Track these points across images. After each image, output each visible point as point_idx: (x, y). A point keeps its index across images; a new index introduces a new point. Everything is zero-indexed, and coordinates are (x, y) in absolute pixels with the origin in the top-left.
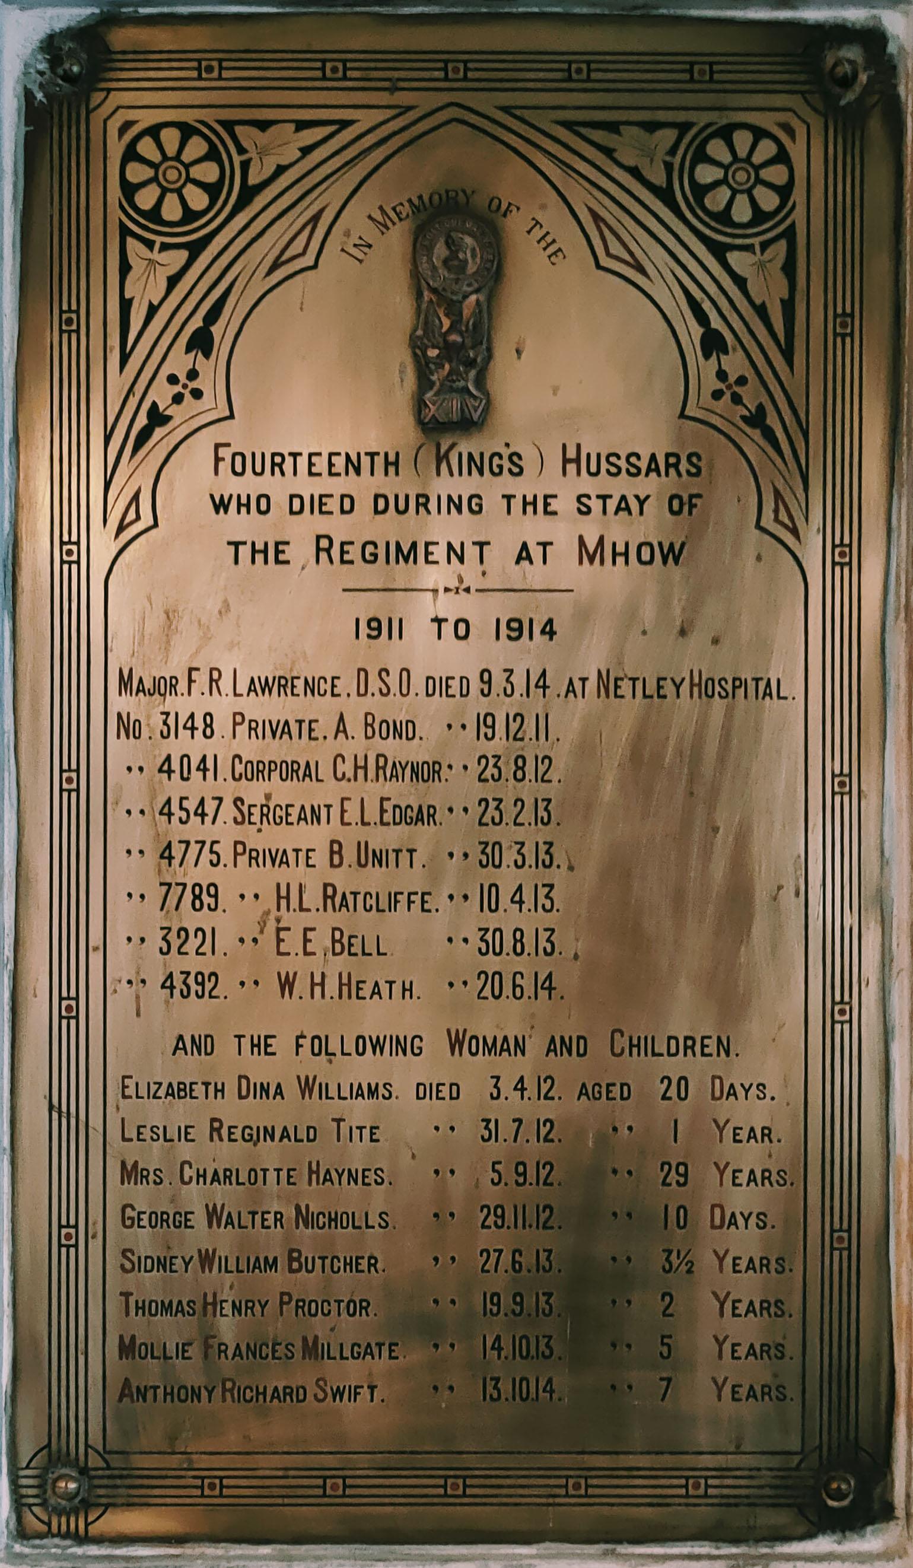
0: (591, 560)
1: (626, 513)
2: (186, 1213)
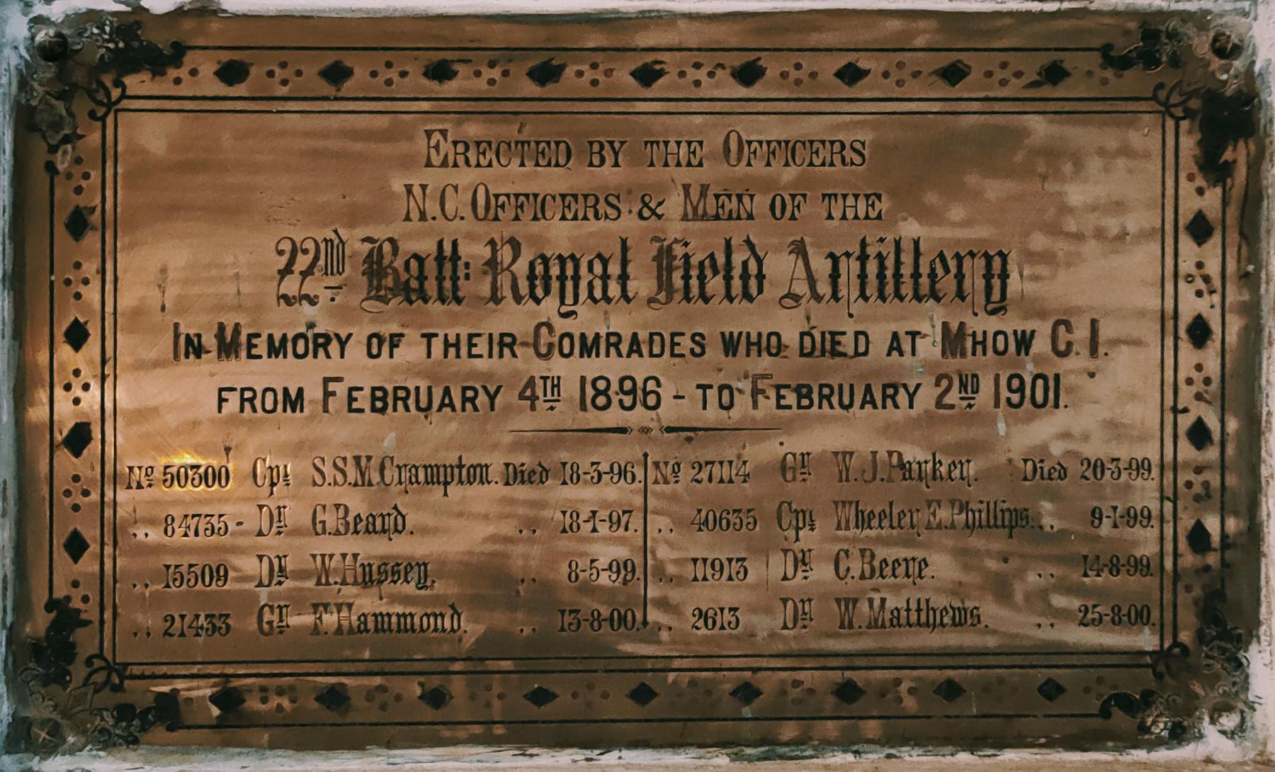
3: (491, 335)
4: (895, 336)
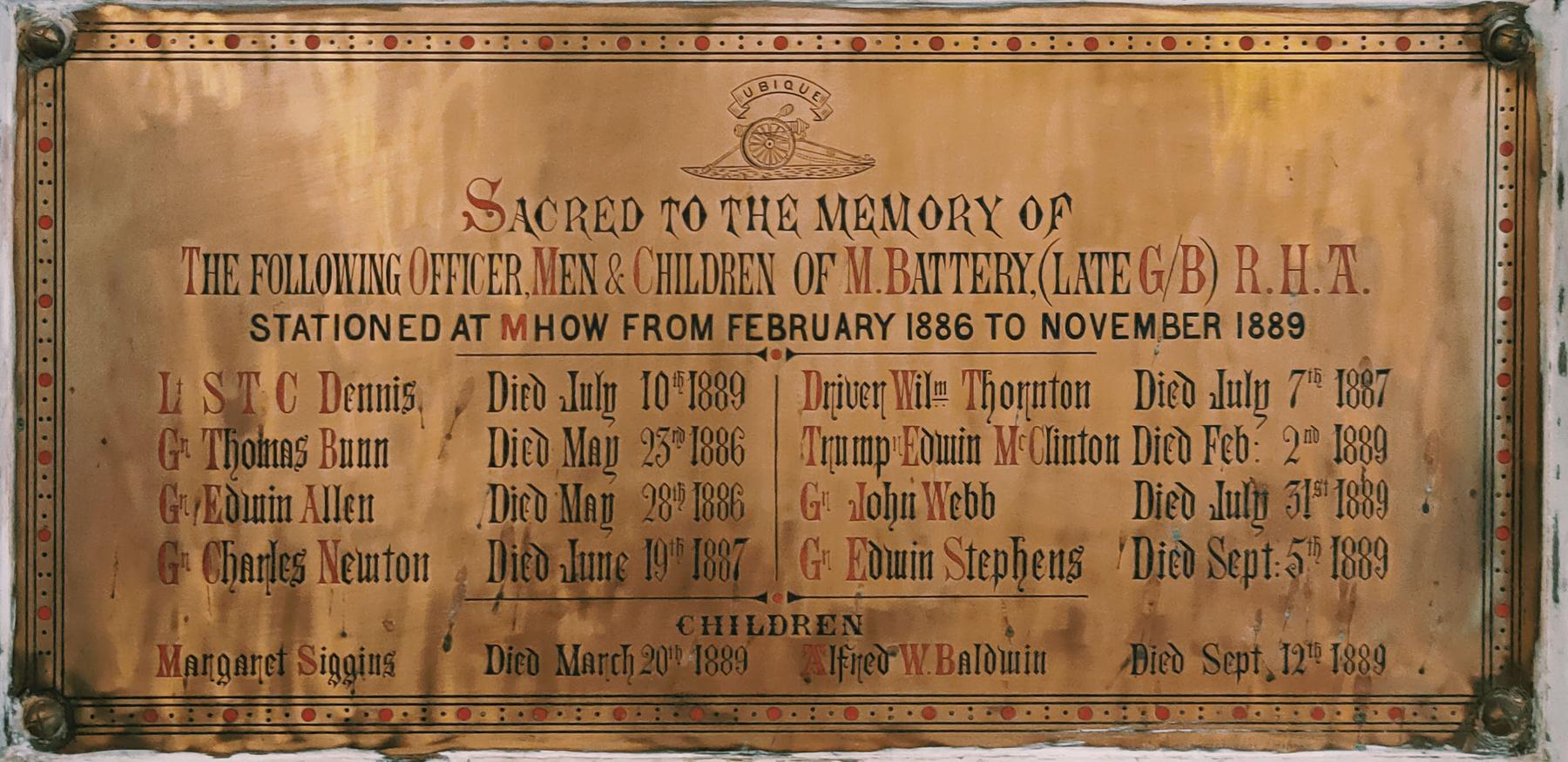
2: (750, 317)
3: (337, 316)
4: (462, 319)
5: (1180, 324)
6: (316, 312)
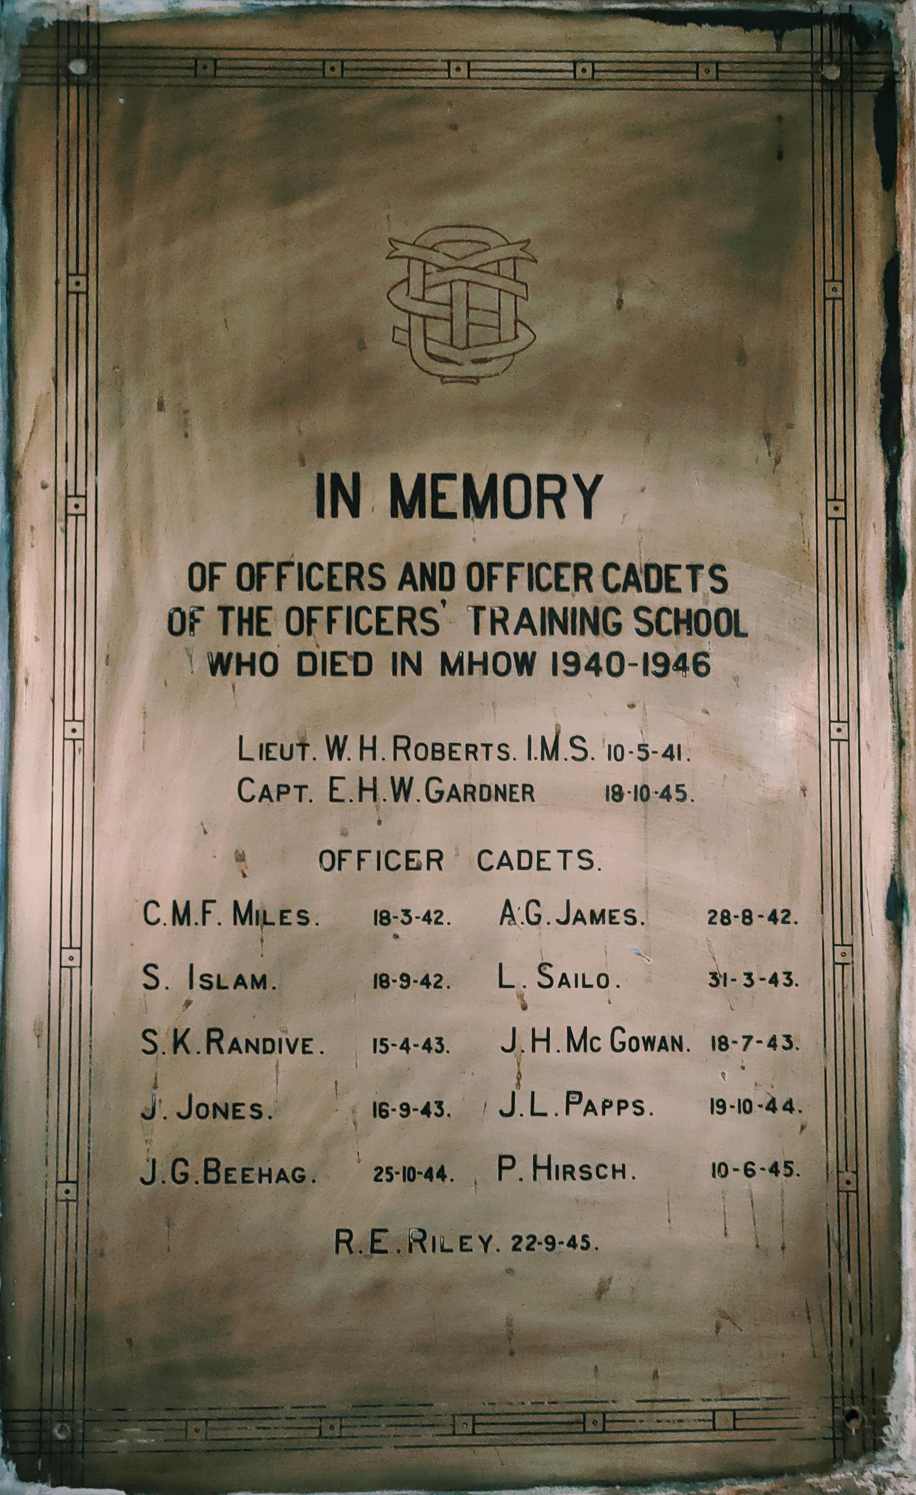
0: (243, 922)
1: (529, 630)
5: (446, 751)
6: (223, 604)
